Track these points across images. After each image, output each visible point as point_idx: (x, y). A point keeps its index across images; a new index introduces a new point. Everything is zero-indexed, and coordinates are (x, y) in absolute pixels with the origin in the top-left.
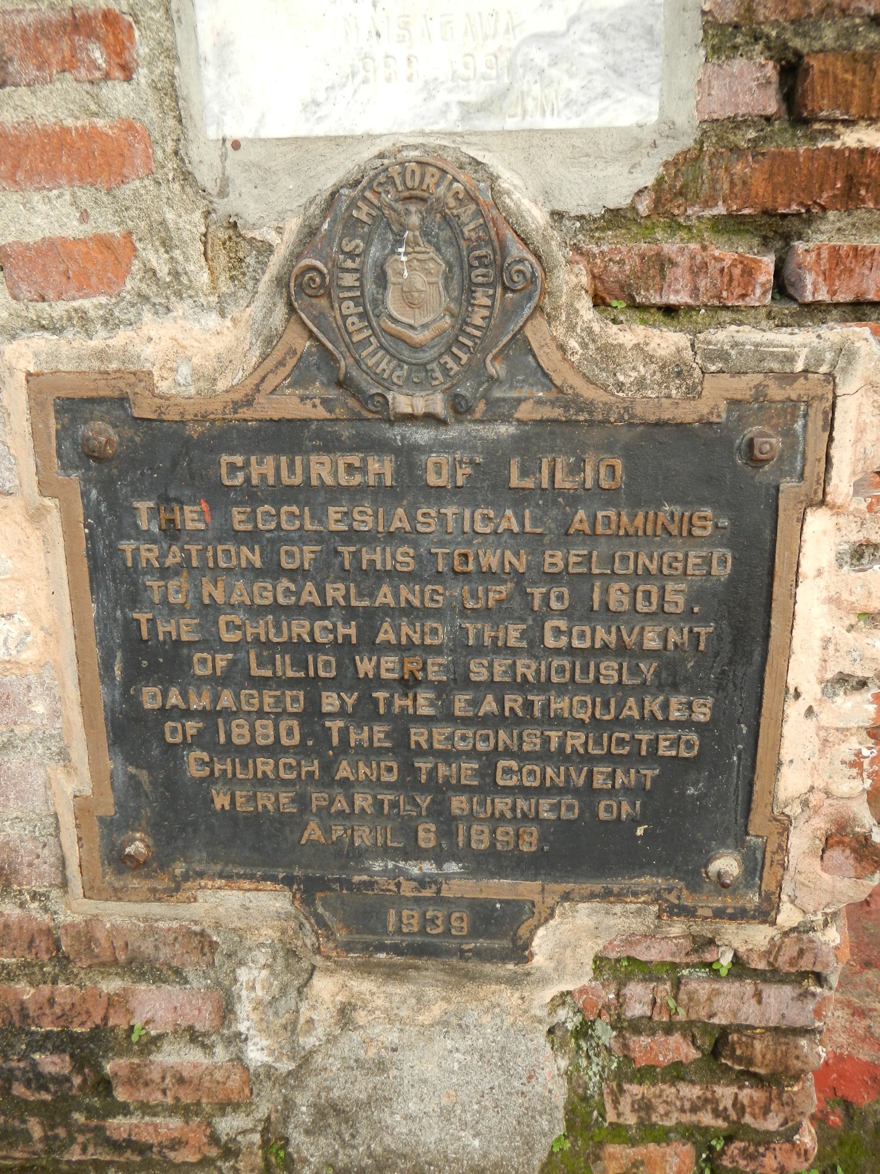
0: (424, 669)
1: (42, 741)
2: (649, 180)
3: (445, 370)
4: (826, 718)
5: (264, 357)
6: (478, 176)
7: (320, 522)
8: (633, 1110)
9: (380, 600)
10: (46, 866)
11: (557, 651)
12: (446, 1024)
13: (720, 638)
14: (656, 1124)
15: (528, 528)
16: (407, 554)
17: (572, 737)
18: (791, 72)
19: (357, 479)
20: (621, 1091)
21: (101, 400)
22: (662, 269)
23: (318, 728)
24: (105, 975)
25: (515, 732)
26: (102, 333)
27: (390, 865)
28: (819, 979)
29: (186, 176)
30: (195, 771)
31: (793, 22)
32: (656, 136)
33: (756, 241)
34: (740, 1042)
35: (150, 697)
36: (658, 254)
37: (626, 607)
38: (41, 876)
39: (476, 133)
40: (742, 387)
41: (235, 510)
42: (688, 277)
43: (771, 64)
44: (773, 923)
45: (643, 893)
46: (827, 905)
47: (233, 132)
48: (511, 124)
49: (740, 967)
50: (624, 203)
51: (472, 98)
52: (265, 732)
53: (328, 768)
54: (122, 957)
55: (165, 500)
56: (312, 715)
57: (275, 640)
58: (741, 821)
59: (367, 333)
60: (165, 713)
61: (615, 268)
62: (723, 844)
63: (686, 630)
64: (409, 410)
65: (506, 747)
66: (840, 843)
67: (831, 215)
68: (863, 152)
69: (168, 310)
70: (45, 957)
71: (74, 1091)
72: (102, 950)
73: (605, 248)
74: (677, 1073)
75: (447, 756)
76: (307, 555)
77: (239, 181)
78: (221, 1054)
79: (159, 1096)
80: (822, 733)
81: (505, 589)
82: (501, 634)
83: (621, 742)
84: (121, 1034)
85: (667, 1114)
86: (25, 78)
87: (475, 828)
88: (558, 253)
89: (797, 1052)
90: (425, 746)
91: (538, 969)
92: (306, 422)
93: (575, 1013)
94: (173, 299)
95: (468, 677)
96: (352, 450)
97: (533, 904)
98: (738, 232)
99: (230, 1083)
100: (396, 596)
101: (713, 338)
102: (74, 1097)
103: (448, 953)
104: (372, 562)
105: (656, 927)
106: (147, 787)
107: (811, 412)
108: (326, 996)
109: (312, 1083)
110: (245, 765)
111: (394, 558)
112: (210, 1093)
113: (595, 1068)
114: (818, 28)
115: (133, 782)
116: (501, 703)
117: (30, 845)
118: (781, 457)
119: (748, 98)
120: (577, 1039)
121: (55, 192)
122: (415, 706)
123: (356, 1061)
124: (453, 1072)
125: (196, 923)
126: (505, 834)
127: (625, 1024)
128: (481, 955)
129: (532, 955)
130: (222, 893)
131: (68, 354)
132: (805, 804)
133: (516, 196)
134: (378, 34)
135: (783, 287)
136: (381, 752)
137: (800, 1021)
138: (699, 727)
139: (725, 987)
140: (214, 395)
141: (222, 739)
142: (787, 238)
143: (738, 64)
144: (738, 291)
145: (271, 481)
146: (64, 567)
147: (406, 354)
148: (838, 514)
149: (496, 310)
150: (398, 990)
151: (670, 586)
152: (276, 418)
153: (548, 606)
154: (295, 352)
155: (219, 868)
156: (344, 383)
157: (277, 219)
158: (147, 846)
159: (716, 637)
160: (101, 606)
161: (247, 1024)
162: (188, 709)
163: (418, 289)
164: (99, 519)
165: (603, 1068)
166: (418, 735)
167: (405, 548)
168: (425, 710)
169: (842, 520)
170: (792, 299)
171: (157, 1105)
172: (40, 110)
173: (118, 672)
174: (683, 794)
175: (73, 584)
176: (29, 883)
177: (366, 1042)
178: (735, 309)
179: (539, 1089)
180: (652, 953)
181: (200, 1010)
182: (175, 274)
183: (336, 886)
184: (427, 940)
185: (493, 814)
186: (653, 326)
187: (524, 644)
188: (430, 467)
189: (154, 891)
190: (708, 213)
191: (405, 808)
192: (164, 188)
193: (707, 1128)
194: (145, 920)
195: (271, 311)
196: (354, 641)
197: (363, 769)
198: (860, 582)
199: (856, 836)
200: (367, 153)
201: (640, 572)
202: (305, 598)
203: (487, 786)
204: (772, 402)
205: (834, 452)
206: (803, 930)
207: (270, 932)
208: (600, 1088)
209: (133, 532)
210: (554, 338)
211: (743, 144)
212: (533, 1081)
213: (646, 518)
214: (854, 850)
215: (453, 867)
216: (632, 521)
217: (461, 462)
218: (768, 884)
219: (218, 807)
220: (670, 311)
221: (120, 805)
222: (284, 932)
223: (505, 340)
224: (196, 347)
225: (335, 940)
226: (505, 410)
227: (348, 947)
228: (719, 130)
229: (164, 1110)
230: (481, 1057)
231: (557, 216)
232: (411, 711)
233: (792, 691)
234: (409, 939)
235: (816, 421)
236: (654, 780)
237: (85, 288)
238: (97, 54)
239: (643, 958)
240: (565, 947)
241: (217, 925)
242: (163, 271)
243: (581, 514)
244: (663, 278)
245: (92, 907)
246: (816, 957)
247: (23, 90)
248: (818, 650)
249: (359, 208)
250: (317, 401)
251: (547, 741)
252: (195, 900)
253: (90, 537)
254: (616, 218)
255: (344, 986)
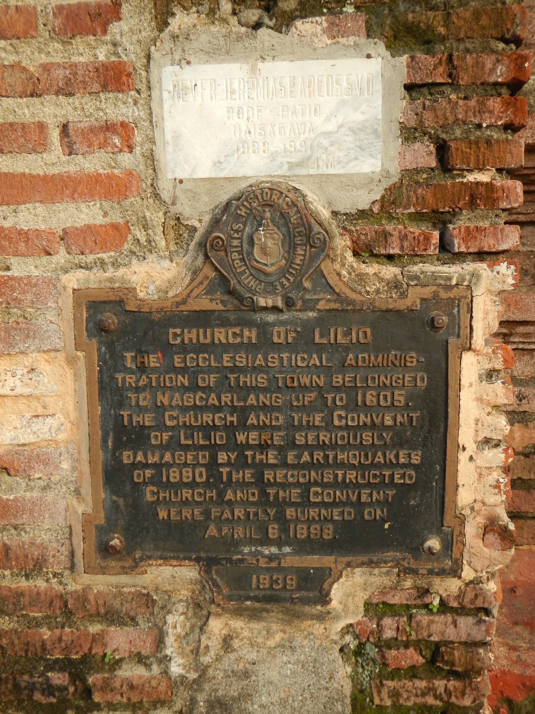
0: (272, 439)
1: (66, 484)
2: (378, 197)
3: (282, 285)
4: (479, 462)
5: (192, 280)
6: (297, 195)
7: (219, 362)
8: (389, 697)
9: (249, 402)
10: (63, 557)
11: (340, 428)
12: (283, 646)
13: (423, 420)
14: (401, 705)
15: (324, 364)
16: (263, 378)
17: (350, 474)
18: (442, 150)
19: (239, 340)
20: (382, 685)
21: (110, 302)
22: (386, 238)
23: (215, 472)
24: (92, 622)
25: (320, 472)
26: (112, 270)
27: (253, 549)
28: (487, 612)
29: (156, 196)
30: (149, 498)
31: (441, 127)
32: (380, 177)
33: (430, 225)
34: (446, 652)
35: (127, 457)
36: (383, 231)
37: (375, 403)
38: (59, 563)
39: (296, 176)
40: (427, 292)
41: (175, 357)
42: (398, 241)
43: (432, 145)
44: (460, 577)
45: (389, 562)
46: (488, 567)
47: (180, 175)
48: (312, 172)
49: (444, 607)
50: (367, 207)
51: (294, 160)
52: (187, 475)
53: (221, 494)
54: (102, 611)
55: (139, 352)
56: (213, 465)
57: (194, 424)
58: (439, 519)
59: (244, 268)
60: (134, 466)
61: (363, 237)
62: (431, 532)
63: (405, 415)
64: (265, 305)
65: (315, 480)
66: (492, 530)
67: (464, 212)
68: (477, 183)
69: (145, 258)
70: (58, 612)
71: (70, 696)
72: (91, 607)
73: (358, 228)
74: (413, 673)
75: (284, 486)
76: (212, 379)
77: (182, 197)
78: (156, 669)
79: (119, 697)
80: (478, 470)
81: (313, 395)
82: (311, 419)
83: (375, 476)
84: (98, 658)
85: (408, 698)
86: (81, 151)
87: (299, 526)
88: (336, 231)
89: (478, 657)
90: (272, 481)
91: (334, 609)
92: (213, 311)
93: (354, 639)
94: (147, 253)
95: (294, 443)
96: (236, 325)
97: (330, 569)
98: (421, 220)
99: (160, 688)
100: (258, 400)
101: (412, 270)
102: (69, 700)
103: (285, 600)
104: (246, 382)
105: (398, 582)
106: (122, 508)
107: (461, 304)
108: (216, 631)
109: (207, 687)
110: (176, 494)
111: (256, 380)
112: (149, 694)
113: (366, 673)
114: (453, 130)
115: (115, 506)
116: (312, 456)
117: (55, 545)
118: (448, 326)
119: (422, 160)
120: (356, 657)
121: (92, 203)
122: (267, 459)
123: (232, 672)
124: (287, 676)
125: (144, 588)
126: (315, 529)
127: (383, 643)
128: (304, 601)
129: (331, 600)
130: (161, 568)
131: (93, 279)
132: (472, 509)
133: (315, 204)
134: (250, 132)
135: (444, 246)
136: (249, 484)
137: (479, 638)
138: (415, 467)
139: (436, 618)
140: (166, 299)
141: (164, 479)
142: (444, 223)
143: (417, 145)
144: (422, 248)
145: (194, 341)
146: (85, 388)
147: (263, 278)
148: (478, 355)
149: (307, 257)
150: (256, 626)
151: (396, 392)
152: (198, 309)
153: (335, 404)
154: (208, 278)
155: (159, 553)
156: (231, 292)
157: (198, 214)
158: (121, 542)
159: (421, 419)
160: (103, 408)
161: (171, 649)
162: (147, 463)
163: (269, 247)
164: (105, 362)
165: (371, 672)
166: (268, 475)
167: (262, 375)
168: (271, 461)
169: (480, 358)
170: (449, 251)
171: (117, 704)
172: (87, 165)
173: (110, 444)
174: (408, 504)
175: (89, 397)
176: (52, 567)
177: (239, 660)
178: (422, 256)
179: (336, 685)
180: (396, 599)
181: (144, 642)
182: (149, 241)
183: (224, 562)
184: (273, 593)
185: (308, 518)
186: (383, 264)
187: (323, 424)
188: (275, 333)
189: (123, 568)
190: (406, 212)
191: (261, 516)
192: (145, 201)
193: (431, 707)
194: (117, 587)
195: (196, 258)
196: (235, 424)
197: (239, 494)
198: (491, 390)
199: (500, 526)
200: (244, 185)
201: (381, 385)
202: (210, 401)
203: (305, 502)
204: (442, 299)
205: (473, 323)
206: (476, 582)
207: (186, 592)
208: (370, 684)
209: (122, 369)
210: (335, 270)
211: (422, 181)
212: (332, 680)
213: (383, 357)
214: (500, 534)
215: (287, 549)
216: (376, 359)
217: (290, 331)
218: (456, 554)
219: (161, 518)
220: (390, 258)
221: (107, 518)
222: (193, 592)
223: (311, 271)
224: (156, 276)
225: (223, 594)
226: (312, 305)
227: (230, 598)
228: (410, 174)
229: (121, 707)
230: (303, 666)
231: (335, 214)
232: (265, 461)
233: (461, 446)
234: (263, 592)
235: (464, 309)
236: (393, 497)
237: (104, 248)
238: (117, 141)
239: (392, 602)
240: (348, 596)
241: (157, 589)
242: (143, 240)
243: (351, 356)
244: (386, 242)
245: (86, 579)
246: (484, 598)
247: (80, 156)
248: (473, 426)
249: (241, 210)
250: (218, 301)
251: (336, 476)
252: (146, 573)
253: (100, 372)
254: (362, 214)
255: (226, 624)
